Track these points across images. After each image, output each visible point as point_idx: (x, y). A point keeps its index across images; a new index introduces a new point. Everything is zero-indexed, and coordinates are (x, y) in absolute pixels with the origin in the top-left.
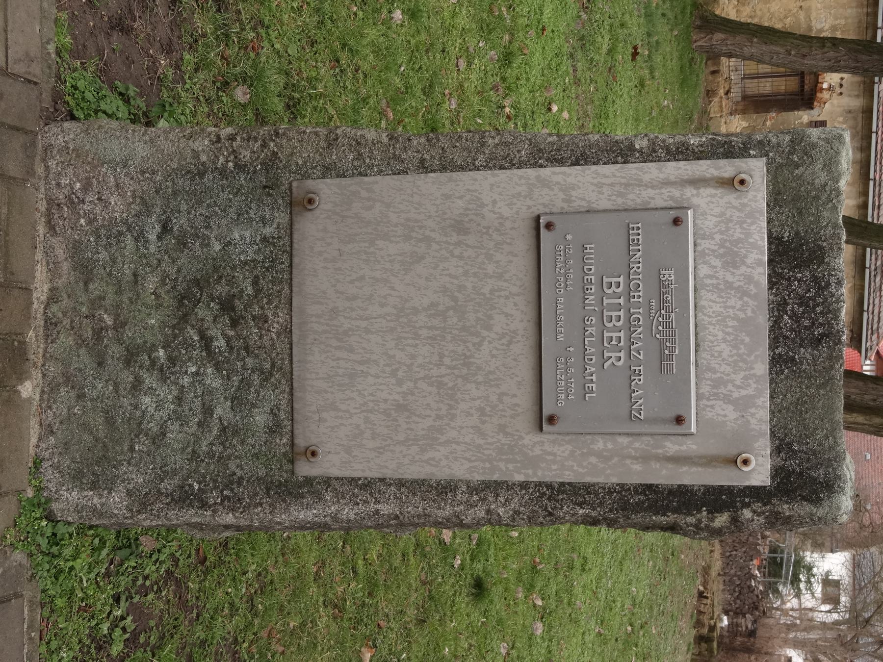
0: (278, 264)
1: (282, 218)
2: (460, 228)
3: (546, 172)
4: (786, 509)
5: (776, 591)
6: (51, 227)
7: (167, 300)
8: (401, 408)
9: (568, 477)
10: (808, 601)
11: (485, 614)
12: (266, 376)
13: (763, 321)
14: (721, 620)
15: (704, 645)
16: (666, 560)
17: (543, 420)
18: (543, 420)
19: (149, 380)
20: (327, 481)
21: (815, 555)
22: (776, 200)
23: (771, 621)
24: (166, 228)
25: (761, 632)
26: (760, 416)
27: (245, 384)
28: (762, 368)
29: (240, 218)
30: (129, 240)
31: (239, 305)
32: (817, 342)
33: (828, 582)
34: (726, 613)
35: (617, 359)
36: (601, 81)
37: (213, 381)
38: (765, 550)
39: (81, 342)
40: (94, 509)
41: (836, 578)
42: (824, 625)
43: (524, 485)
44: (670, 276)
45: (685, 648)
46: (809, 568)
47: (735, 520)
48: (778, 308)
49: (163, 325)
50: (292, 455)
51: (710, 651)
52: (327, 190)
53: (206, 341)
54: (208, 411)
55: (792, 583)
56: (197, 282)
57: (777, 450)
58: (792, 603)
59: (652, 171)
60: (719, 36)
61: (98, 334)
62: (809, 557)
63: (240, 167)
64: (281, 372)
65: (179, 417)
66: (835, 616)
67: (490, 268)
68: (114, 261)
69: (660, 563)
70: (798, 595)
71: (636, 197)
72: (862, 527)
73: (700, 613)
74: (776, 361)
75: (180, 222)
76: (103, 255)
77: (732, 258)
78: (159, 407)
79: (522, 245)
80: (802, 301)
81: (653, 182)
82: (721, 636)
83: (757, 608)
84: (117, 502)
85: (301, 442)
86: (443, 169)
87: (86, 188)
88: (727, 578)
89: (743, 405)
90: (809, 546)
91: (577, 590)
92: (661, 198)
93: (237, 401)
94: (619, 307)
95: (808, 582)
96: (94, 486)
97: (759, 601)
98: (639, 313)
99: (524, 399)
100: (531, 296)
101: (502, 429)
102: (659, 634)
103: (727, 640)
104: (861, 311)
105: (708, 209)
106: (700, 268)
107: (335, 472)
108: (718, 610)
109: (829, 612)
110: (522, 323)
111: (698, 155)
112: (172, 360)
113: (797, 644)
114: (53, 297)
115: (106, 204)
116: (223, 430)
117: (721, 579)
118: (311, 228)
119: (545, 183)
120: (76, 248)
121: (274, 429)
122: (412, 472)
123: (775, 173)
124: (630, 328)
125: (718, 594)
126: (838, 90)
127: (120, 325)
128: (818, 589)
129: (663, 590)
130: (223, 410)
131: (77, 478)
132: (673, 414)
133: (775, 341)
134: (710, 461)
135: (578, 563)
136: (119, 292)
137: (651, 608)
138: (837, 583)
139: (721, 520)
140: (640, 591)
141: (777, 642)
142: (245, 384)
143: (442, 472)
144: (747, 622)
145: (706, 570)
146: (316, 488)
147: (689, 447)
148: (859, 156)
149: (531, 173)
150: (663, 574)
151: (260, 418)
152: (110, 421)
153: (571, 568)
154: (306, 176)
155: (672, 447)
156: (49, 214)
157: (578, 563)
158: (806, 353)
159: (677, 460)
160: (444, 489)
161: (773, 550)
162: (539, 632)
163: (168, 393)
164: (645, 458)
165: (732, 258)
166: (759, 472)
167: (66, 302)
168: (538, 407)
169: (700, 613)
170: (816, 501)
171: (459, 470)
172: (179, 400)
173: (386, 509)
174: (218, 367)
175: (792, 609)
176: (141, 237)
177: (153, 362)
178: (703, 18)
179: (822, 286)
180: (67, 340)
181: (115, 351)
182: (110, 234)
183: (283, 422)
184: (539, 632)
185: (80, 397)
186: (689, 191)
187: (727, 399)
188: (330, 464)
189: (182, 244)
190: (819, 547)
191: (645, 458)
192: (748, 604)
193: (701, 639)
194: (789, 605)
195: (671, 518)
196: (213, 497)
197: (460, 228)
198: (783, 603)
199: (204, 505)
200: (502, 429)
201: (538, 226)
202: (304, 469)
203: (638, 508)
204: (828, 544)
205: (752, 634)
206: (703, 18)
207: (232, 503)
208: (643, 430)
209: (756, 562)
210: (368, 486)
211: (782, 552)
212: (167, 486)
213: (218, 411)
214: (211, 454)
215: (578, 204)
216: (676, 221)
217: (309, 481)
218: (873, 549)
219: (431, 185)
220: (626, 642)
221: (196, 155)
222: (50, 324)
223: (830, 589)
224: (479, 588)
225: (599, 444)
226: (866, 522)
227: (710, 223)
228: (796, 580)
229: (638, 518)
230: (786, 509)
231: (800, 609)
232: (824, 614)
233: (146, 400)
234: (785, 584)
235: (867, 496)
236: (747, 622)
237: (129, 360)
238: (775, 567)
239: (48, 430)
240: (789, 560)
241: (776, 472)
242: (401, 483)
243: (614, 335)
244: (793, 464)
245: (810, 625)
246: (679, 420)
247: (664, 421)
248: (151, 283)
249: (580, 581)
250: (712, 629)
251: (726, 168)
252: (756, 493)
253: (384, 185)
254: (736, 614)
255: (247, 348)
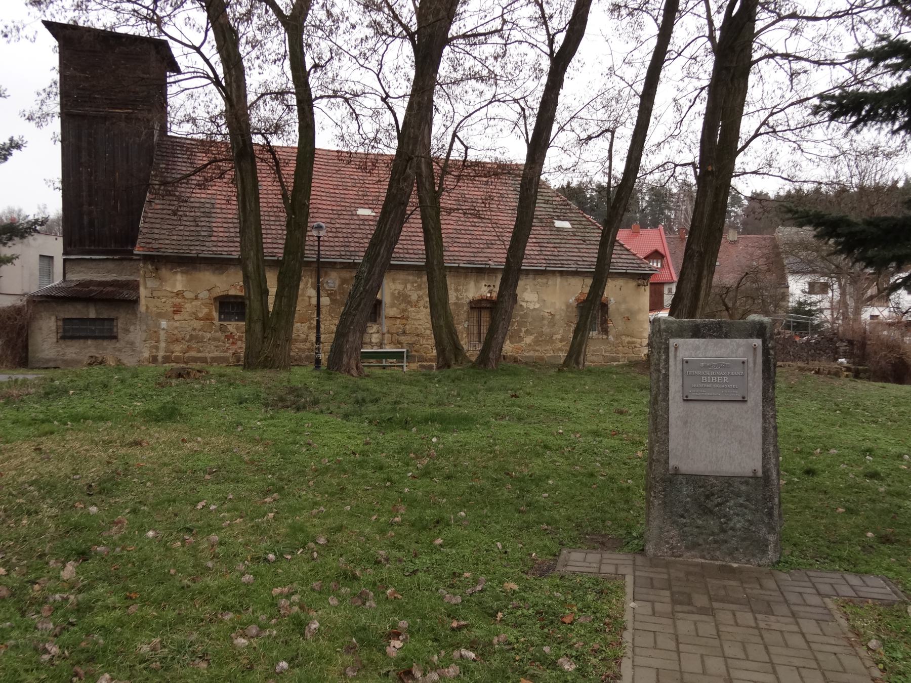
0: (695, 480)
1: (680, 478)
2: (686, 423)
3: (670, 398)
4: (768, 335)
5: (819, 326)
6: (680, 556)
7: (705, 518)
8: (740, 442)
9: (760, 394)
10: (826, 304)
11: (824, 471)
12: (730, 485)
13: (715, 340)
14: (842, 363)
15: (861, 375)
16: (794, 391)
17: (744, 401)
18: (744, 401)
19: (731, 524)
20: (764, 467)
21: (791, 299)
22: (681, 336)
23: (841, 329)
24: (682, 516)
25: (849, 337)
26: (742, 341)
27: (732, 492)
28: (728, 341)
29: (680, 491)
30: (685, 529)
31: (707, 493)
32: (721, 327)
33: (813, 288)
34: (837, 359)
35: (726, 379)
36: (536, 412)
37: (732, 503)
38: (788, 333)
39: (719, 549)
40: (775, 546)
41: (807, 286)
42: (843, 294)
43: (763, 407)
44: (702, 364)
45: (853, 383)
46: (800, 303)
47: (772, 348)
48: (711, 336)
49: (713, 519)
51: (865, 371)
52: (673, 463)
53: (719, 505)
54: (741, 505)
55: (813, 315)
56: (700, 506)
57: (751, 337)
58: (827, 315)
59: (672, 369)
60: (491, 355)
61: (715, 542)
62: (792, 303)
63: (664, 490)
64: (729, 480)
65: (744, 515)
66: (836, 286)
67: (698, 414)
68: (692, 534)
69: (797, 395)
70: (821, 311)
71: (679, 373)
72: (769, 270)
73: (829, 373)
74: (726, 337)
75: (681, 511)
76: (690, 538)
77: (697, 348)
78: (739, 521)
79: (691, 404)
80: (709, 330)
81: (675, 369)
82: (854, 363)
83: (831, 339)
84: (772, 538)
85: (751, 475)
86: (668, 427)
87: (667, 543)
88: (810, 358)
89: (739, 346)
90: (784, 303)
91: (812, 434)
92: (679, 367)
93: (738, 495)
95: (810, 304)
96: (767, 546)
97: (826, 337)
98: (712, 373)
99: (737, 405)
100: (706, 403)
101: (746, 412)
102: (843, 397)
103: (857, 360)
104: (626, 273)
105: (683, 354)
106: (700, 356)
107: (760, 464)
108: (834, 365)
109: (832, 290)
110: (714, 406)
111: (668, 356)
112: (725, 516)
113: (858, 312)
114: (703, 557)
115: (673, 536)
116: (747, 500)
117: (811, 362)
118: (685, 468)
119: (674, 398)
120: (688, 548)
121: (747, 483)
122: (760, 440)
123: (674, 337)
125: (824, 364)
126: (492, 288)
127: (713, 534)
128: (815, 298)
129: (814, 394)
130: (741, 500)
131: (764, 552)
133: (719, 337)
134: (755, 355)
135: (796, 433)
136: (702, 533)
137: (826, 400)
138: (812, 285)
139: (772, 352)
140: (814, 406)
141: (856, 326)
142: (732, 492)
143: (760, 431)
144: (843, 346)
145: (801, 369)
146: (766, 470)
147: (751, 360)
148: (531, 276)
149: (670, 402)
150: (804, 394)
151: (743, 488)
152: (744, 540)
153: (799, 436)
154: (668, 469)
155: (751, 365)
156: (676, 557)
157: (796, 433)
158: (724, 329)
159: (755, 363)
160: (765, 430)
161: (788, 327)
162: (836, 451)
163: (736, 519)
164: (754, 372)
165: (697, 348)
166: (758, 342)
167: (705, 553)
169: (829, 373)
170: (765, 327)
171: (759, 425)
172: (738, 515)
173: (772, 449)
174: (727, 501)
175: (832, 315)
176: (685, 525)
177: (725, 523)
178: (480, 363)
179: (705, 325)
180: (718, 553)
181: (722, 536)
182: (683, 536)
183: (744, 480)
184: (836, 451)
185: (737, 549)
186: (678, 359)
187: (737, 350)
188: (758, 466)
189: (687, 511)
190: (785, 296)
191: (754, 372)
192: (828, 344)
193: (857, 375)
194: (829, 317)
195: (772, 365)
196: (770, 504)
197: (686, 423)
198: (827, 321)
199: (772, 508)
200: (746, 412)
201: (686, 400)
202: (760, 474)
203: (769, 375)
204: (782, 290)
205: (851, 343)
206: (480, 363)
207: (771, 498)
209: (797, 339)
210: (765, 454)
211: (789, 322)
212: (766, 520)
213: (741, 502)
214: (755, 505)
215: (681, 388)
216: (687, 362)
217: (763, 472)
218: (786, 262)
219: (673, 431)
220: (846, 414)
221: (659, 504)
222: (712, 558)
223: (817, 289)
224: (810, 472)
225: (750, 385)
226: (765, 267)
227: (687, 354)
228: (810, 313)
229: (772, 375)
230: (768, 335)
231: (832, 308)
232: (835, 293)
233: (738, 526)
234: (812, 320)
235: (747, 266)
236: (843, 346)
237: (724, 531)
238: (801, 327)
239: (748, 562)
240: (795, 318)
241: (758, 337)
242: (764, 443)
244: (755, 333)
245: (843, 303)
246: (743, 363)
247: (744, 368)
248: (700, 522)
249: (807, 432)
250: (848, 369)
251: (672, 349)
252: (764, 342)
253: (672, 445)
254: (837, 353)
255: (721, 491)
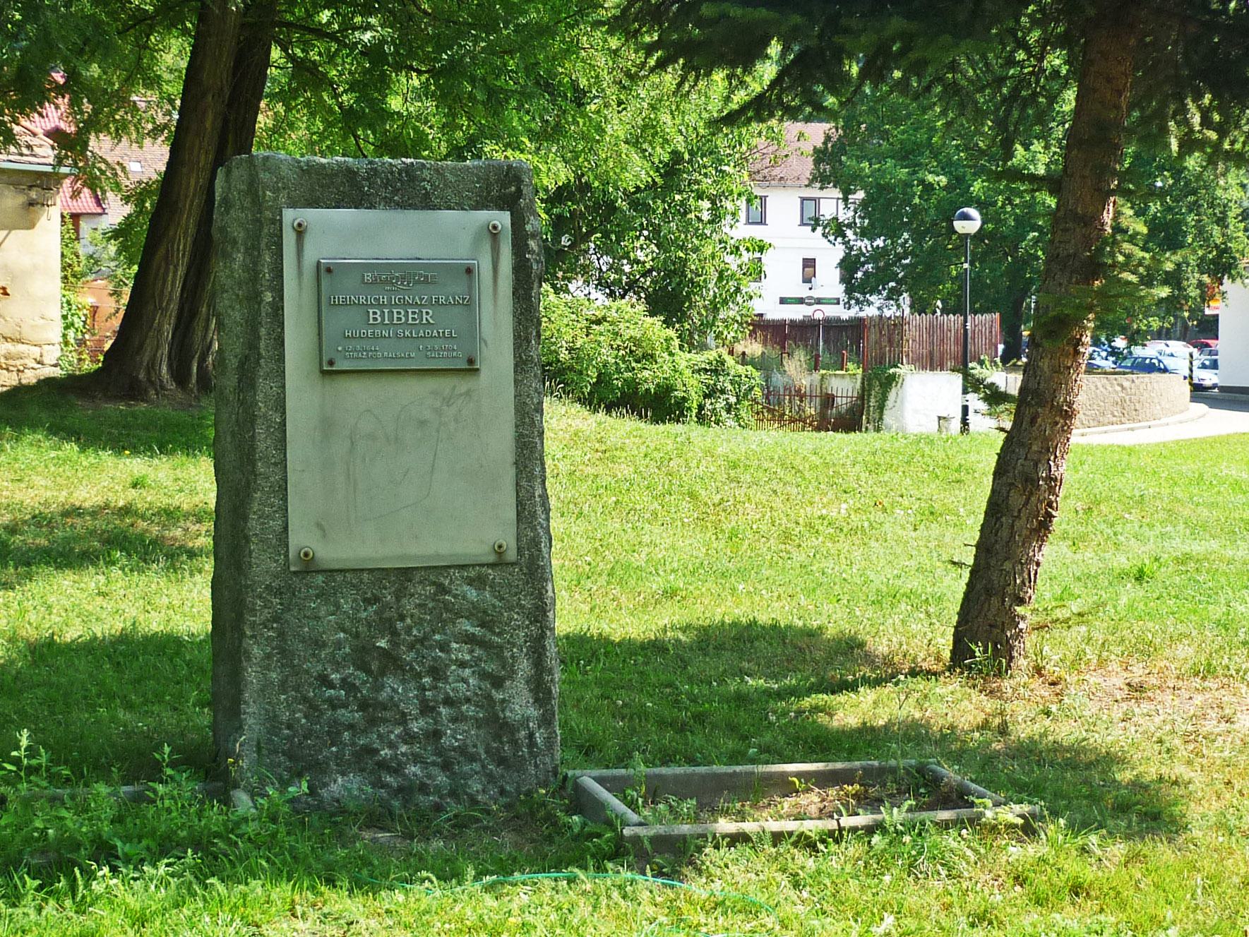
18: (471, 369)
48: (390, 203)
50: (500, 562)
85: (492, 558)
94: (391, 313)
106: (359, 253)
121: (479, 582)
124: (406, 305)
132: (465, 277)
166: (503, 219)
168: (316, 339)
183: (475, 573)
202: (512, 555)
208: (500, 302)
216: (329, 270)
243: (410, 316)
251: (289, 239)
